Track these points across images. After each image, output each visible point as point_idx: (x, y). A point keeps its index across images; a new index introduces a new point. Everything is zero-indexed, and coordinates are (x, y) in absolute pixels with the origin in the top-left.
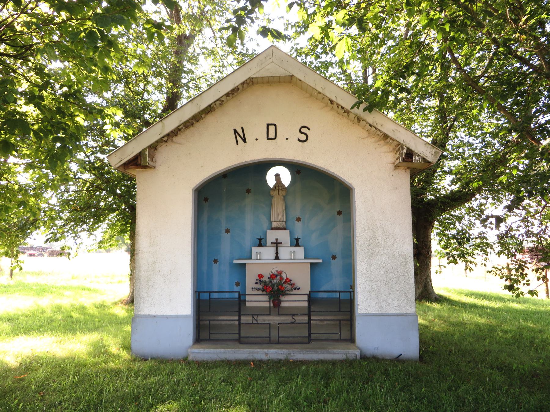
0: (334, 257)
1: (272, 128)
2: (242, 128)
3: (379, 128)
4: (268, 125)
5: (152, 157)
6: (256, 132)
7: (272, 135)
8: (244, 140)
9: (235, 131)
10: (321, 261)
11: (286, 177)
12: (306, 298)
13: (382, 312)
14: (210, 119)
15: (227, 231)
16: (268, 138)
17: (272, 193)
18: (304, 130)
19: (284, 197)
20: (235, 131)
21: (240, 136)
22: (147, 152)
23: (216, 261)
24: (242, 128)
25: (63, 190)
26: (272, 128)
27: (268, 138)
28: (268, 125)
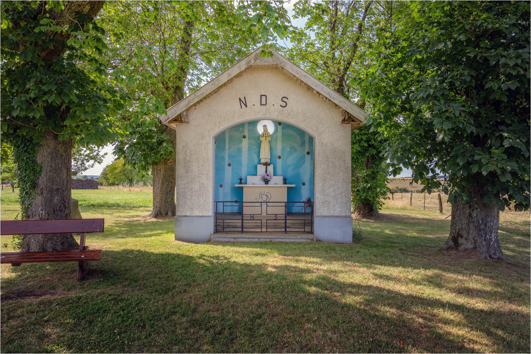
0: (304, 184)
1: (264, 98)
2: (245, 98)
3: (332, 100)
4: (261, 96)
5: (187, 115)
6: (253, 100)
7: (264, 102)
8: (246, 106)
9: (240, 99)
10: (294, 186)
11: (271, 129)
12: (284, 204)
13: (331, 215)
14: (223, 91)
15: (229, 165)
16: (261, 105)
17: (261, 139)
18: (284, 99)
19: (269, 142)
20: (240, 99)
21: (243, 102)
22: (184, 113)
23: (221, 186)
24: (245, 98)
25: (27, 130)
26: (264, 98)
27: (261, 105)
28: (261, 96)
